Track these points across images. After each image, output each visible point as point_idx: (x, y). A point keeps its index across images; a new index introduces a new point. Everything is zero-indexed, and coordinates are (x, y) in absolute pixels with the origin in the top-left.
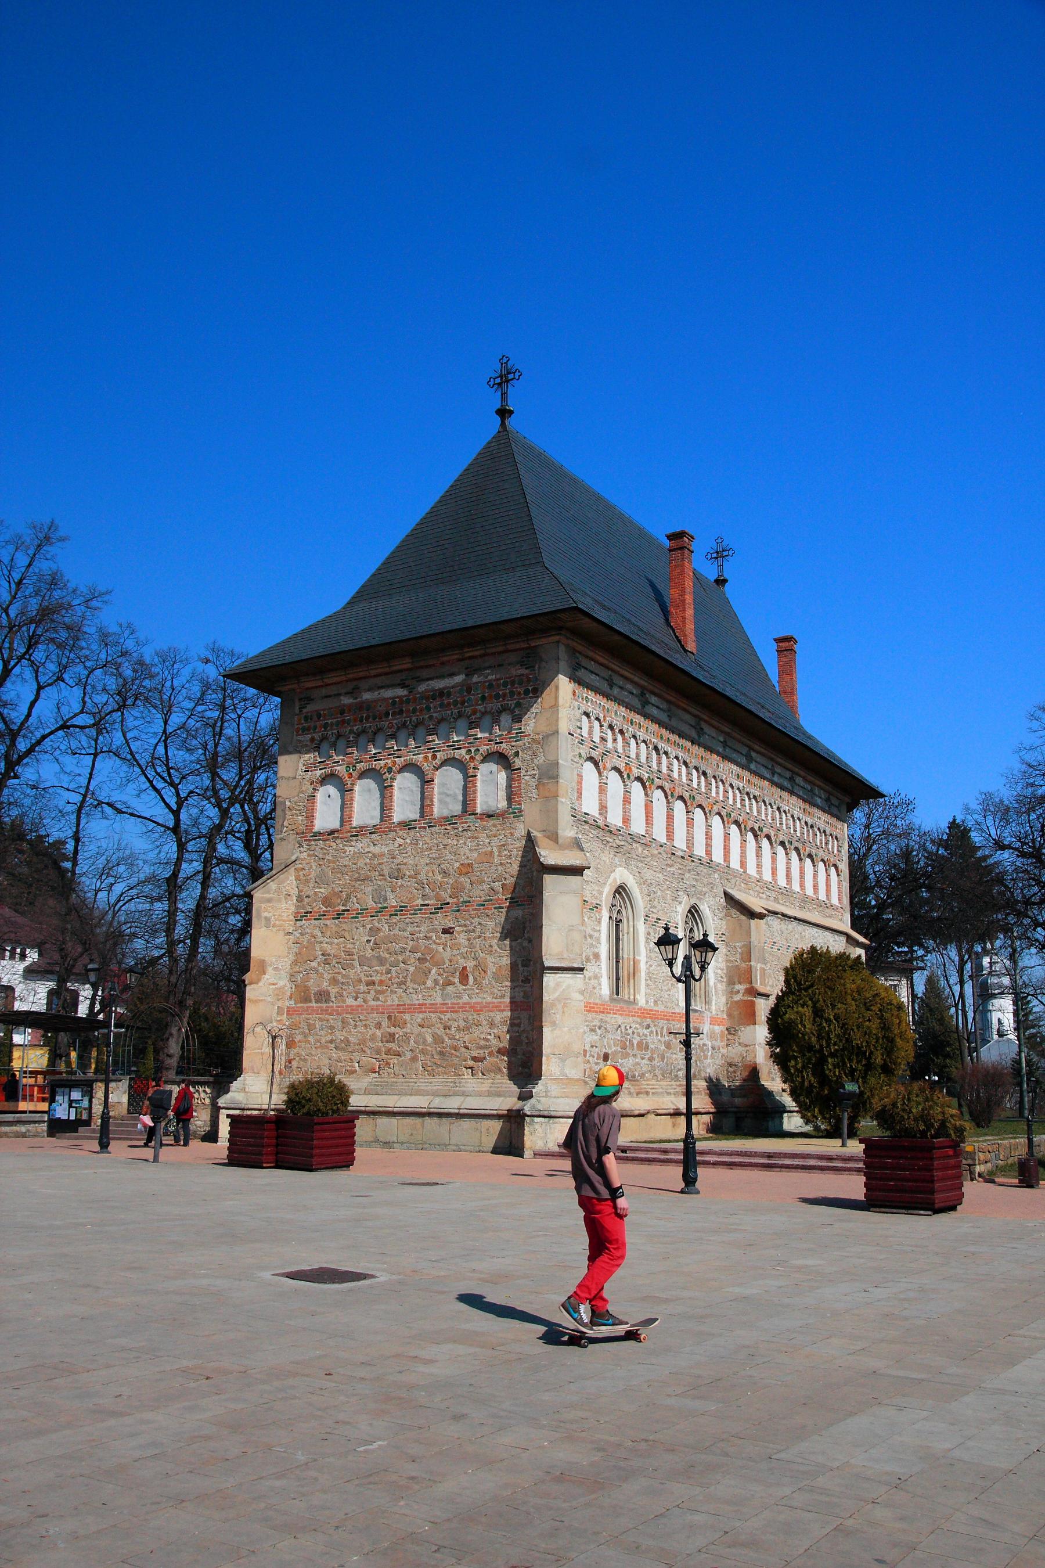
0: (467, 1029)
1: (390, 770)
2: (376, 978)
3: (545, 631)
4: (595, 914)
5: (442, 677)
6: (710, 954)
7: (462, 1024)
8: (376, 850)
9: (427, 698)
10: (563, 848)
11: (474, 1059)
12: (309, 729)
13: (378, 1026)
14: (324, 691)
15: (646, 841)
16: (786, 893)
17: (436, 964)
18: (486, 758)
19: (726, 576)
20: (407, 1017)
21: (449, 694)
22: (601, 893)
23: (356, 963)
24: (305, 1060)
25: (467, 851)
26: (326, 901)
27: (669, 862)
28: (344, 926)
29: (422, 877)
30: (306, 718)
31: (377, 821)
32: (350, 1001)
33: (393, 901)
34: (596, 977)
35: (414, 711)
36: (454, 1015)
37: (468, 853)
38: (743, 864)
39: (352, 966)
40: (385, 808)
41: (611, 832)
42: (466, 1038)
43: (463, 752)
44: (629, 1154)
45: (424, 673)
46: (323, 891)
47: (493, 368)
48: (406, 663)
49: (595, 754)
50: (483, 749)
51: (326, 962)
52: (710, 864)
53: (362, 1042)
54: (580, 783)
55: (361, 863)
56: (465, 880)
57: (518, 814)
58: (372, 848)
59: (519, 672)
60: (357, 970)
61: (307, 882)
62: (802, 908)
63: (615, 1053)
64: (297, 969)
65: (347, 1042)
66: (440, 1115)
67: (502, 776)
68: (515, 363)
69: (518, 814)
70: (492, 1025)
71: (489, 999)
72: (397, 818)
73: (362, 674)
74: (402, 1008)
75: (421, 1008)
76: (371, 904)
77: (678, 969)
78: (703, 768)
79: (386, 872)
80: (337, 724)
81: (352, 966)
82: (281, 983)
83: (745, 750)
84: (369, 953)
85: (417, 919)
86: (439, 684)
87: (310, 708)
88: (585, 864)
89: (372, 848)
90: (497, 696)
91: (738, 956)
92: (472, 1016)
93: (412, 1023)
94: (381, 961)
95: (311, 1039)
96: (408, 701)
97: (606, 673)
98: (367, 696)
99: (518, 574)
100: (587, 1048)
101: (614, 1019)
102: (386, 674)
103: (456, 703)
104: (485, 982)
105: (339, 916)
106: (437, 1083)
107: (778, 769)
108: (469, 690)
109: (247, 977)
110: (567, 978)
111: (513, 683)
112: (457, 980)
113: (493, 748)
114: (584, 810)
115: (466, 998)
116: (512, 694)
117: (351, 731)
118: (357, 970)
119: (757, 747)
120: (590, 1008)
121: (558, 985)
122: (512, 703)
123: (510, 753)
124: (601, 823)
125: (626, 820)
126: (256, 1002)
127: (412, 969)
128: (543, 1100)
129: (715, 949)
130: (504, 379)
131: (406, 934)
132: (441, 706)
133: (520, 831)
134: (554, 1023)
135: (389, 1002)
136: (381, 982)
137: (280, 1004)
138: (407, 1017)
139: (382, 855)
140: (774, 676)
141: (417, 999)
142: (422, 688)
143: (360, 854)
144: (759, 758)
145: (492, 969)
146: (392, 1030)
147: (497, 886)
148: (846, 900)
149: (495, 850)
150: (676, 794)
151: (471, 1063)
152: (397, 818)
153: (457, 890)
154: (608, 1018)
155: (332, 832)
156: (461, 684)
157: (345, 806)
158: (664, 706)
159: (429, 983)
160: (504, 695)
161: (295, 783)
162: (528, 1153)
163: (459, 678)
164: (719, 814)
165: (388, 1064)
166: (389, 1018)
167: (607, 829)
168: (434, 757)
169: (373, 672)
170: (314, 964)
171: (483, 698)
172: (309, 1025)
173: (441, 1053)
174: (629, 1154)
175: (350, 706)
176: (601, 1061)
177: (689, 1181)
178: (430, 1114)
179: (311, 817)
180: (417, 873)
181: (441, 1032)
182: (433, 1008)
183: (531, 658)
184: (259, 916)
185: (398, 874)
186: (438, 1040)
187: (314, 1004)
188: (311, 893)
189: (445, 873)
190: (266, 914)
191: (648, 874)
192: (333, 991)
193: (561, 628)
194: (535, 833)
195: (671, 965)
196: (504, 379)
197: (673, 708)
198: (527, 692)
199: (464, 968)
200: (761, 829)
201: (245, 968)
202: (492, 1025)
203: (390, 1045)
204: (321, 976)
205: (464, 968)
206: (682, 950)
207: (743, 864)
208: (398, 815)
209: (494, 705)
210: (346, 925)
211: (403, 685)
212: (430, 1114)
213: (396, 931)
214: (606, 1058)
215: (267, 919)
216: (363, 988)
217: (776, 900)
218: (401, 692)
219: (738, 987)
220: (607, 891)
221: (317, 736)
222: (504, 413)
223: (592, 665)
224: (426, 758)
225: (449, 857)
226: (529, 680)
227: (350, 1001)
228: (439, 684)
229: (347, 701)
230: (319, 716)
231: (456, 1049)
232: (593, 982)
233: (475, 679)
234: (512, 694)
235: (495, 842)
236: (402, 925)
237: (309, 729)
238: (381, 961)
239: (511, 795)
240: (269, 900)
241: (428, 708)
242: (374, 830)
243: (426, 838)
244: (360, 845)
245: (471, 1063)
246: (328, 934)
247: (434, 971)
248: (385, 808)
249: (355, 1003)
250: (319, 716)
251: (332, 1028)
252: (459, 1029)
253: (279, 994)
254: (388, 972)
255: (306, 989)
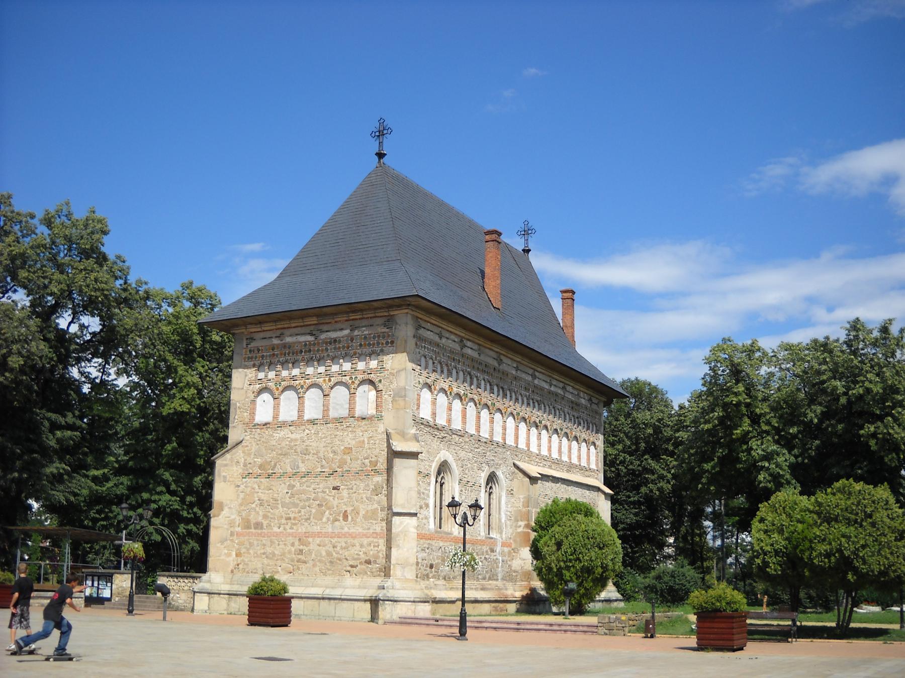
0: (346, 548)
1: (302, 387)
2: (292, 516)
3: (399, 306)
4: (427, 480)
5: (335, 330)
6: (478, 511)
7: (344, 545)
8: (293, 436)
9: (326, 343)
10: (406, 440)
11: (352, 566)
12: (252, 358)
13: (293, 545)
14: (262, 335)
15: (461, 434)
16: (557, 463)
17: (329, 508)
18: (362, 383)
19: (530, 247)
20: (310, 540)
21: (340, 342)
22: (431, 466)
23: (280, 506)
24: (247, 564)
25: (348, 439)
26: (261, 467)
27: (477, 446)
28: (273, 483)
29: (321, 455)
30: (250, 351)
31: (296, 418)
32: (276, 529)
33: (303, 469)
34: (426, 518)
35: (318, 350)
36: (340, 540)
37: (350, 441)
38: (528, 445)
39: (277, 508)
40: (301, 411)
41: (438, 429)
42: (346, 553)
43: (348, 378)
44: (439, 623)
45: (325, 328)
46: (259, 461)
47: (374, 126)
48: (314, 320)
49: (429, 381)
50: (360, 377)
51: (261, 505)
52: (504, 445)
53: (283, 554)
54: (419, 400)
55: (283, 444)
56: (347, 457)
57: (380, 418)
58: (290, 435)
59: (383, 330)
60: (280, 510)
61: (249, 454)
62: (568, 471)
63: (438, 563)
64: (243, 508)
65: (274, 554)
66: (330, 599)
67: (373, 393)
68: (389, 123)
69: (380, 418)
70: (362, 546)
71: (360, 530)
72: (306, 417)
73: (286, 326)
74: (307, 535)
75: (319, 535)
76: (289, 470)
77: (459, 519)
78: (501, 385)
79: (299, 450)
80: (270, 356)
81: (277, 508)
82: (233, 517)
83: (531, 372)
84: (287, 500)
85: (317, 480)
86: (333, 335)
87: (253, 345)
88: (420, 451)
89: (290, 435)
90: (369, 345)
91: (521, 504)
92: (350, 540)
93: (314, 544)
94: (296, 505)
95: (251, 551)
96: (314, 344)
97: (438, 330)
98: (289, 340)
99: (385, 267)
100: (420, 560)
101: (436, 544)
102: (301, 326)
103: (344, 347)
104: (358, 520)
105: (269, 476)
106: (328, 580)
107: (554, 382)
108: (352, 340)
109: (212, 513)
110: (407, 519)
111: (379, 336)
112: (341, 518)
113: (366, 376)
114: (421, 416)
115: (346, 529)
116: (378, 343)
117: (279, 361)
118: (280, 510)
119: (539, 369)
120: (421, 536)
121: (401, 523)
122: (378, 349)
123: (376, 381)
124: (432, 423)
125: (449, 421)
126: (216, 528)
127: (314, 511)
128: (391, 591)
129: (482, 509)
130: (381, 133)
131: (311, 489)
132: (335, 348)
133: (381, 428)
134: (398, 546)
135: (300, 530)
136: (295, 518)
137: (232, 529)
138: (310, 540)
139: (296, 440)
140: (560, 317)
141: (316, 529)
142: (323, 336)
143: (284, 439)
144: (541, 376)
145: (362, 512)
146: (301, 547)
147: (367, 461)
148: (601, 465)
149: (366, 440)
150: (482, 403)
151: (349, 568)
152: (306, 417)
153: (342, 463)
154: (433, 542)
155: (266, 424)
156: (347, 336)
157: (276, 408)
158: (476, 347)
159: (324, 520)
160: (374, 344)
161: (243, 392)
162: (380, 622)
163: (346, 332)
164: (512, 414)
165: (298, 569)
166: (300, 540)
167: (436, 427)
168: (330, 380)
169: (293, 325)
170: (254, 506)
171: (361, 345)
172: (250, 543)
173: (331, 562)
174: (439, 623)
175: (278, 345)
176: (428, 569)
177: (463, 633)
178: (323, 598)
179: (253, 414)
180: (318, 452)
181: (331, 549)
182: (326, 535)
183: (390, 322)
184: (219, 475)
185: (306, 452)
186: (329, 554)
187: (253, 530)
188: (252, 461)
189: (334, 452)
190: (224, 474)
191: (462, 454)
192: (265, 523)
193: (409, 305)
194: (390, 431)
195: (455, 518)
196: (381, 133)
197: (482, 348)
198: (387, 343)
199: (346, 511)
200: (540, 422)
201: (210, 508)
202: (362, 546)
203: (300, 557)
204: (258, 513)
205: (346, 511)
206: (464, 509)
207: (528, 445)
208: (307, 416)
209: (368, 350)
210: (274, 482)
211: (311, 334)
212: (323, 598)
213: (305, 487)
214: (431, 566)
215: (225, 477)
216: (283, 521)
217: (550, 467)
218: (310, 338)
219: (520, 523)
220: (434, 467)
221: (257, 363)
222: (381, 155)
223: (429, 326)
224: (325, 380)
225: (338, 443)
226: (389, 336)
227: (276, 529)
228: (333, 335)
229: (276, 341)
230: (259, 350)
231: (340, 560)
232: (424, 521)
233: (356, 333)
234: (378, 343)
235: (366, 435)
236: (308, 484)
237: (252, 358)
238: (296, 505)
239: (378, 406)
240: (226, 465)
241: (327, 350)
242: (292, 424)
243: (323, 430)
244: (282, 433)
245: (349, 568)
246: (262, 487)
247: (327, 512)
248: (301, 411)
249: (278, 530)
250: (259, 350)
251: (264, 545)
252: (342, 548)
253: (232, 524)
254: (300, 512)
255: (248, 521)
